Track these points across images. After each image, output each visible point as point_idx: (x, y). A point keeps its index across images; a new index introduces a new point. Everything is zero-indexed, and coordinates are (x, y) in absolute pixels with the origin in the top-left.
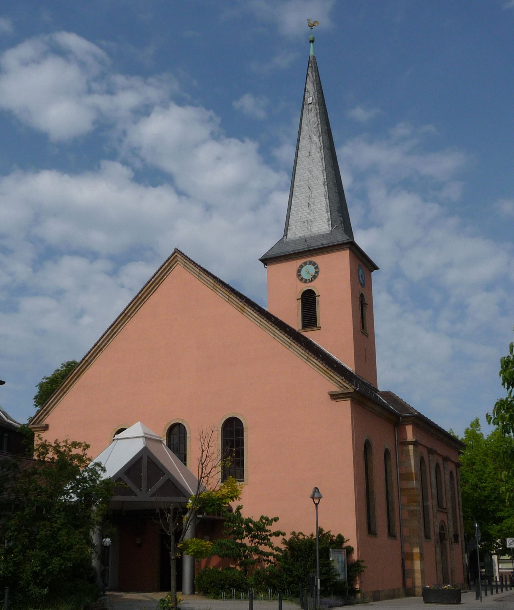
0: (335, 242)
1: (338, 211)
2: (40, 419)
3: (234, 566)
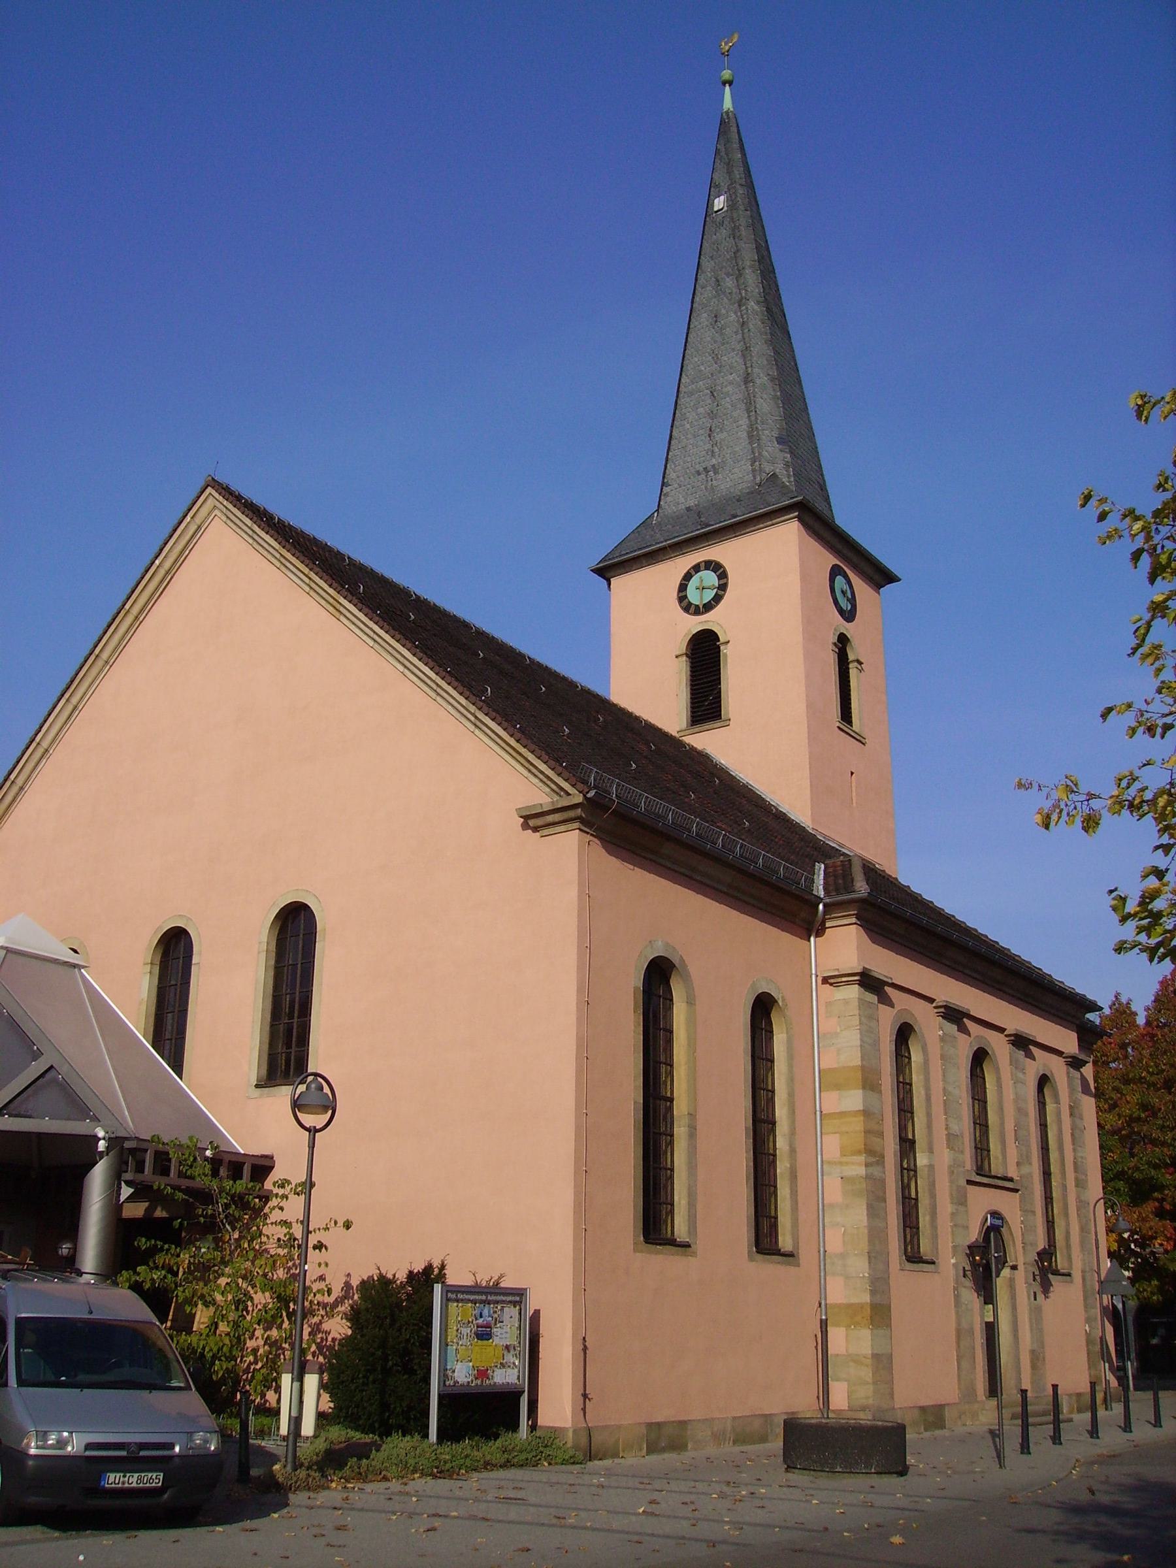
1: (780, 440)
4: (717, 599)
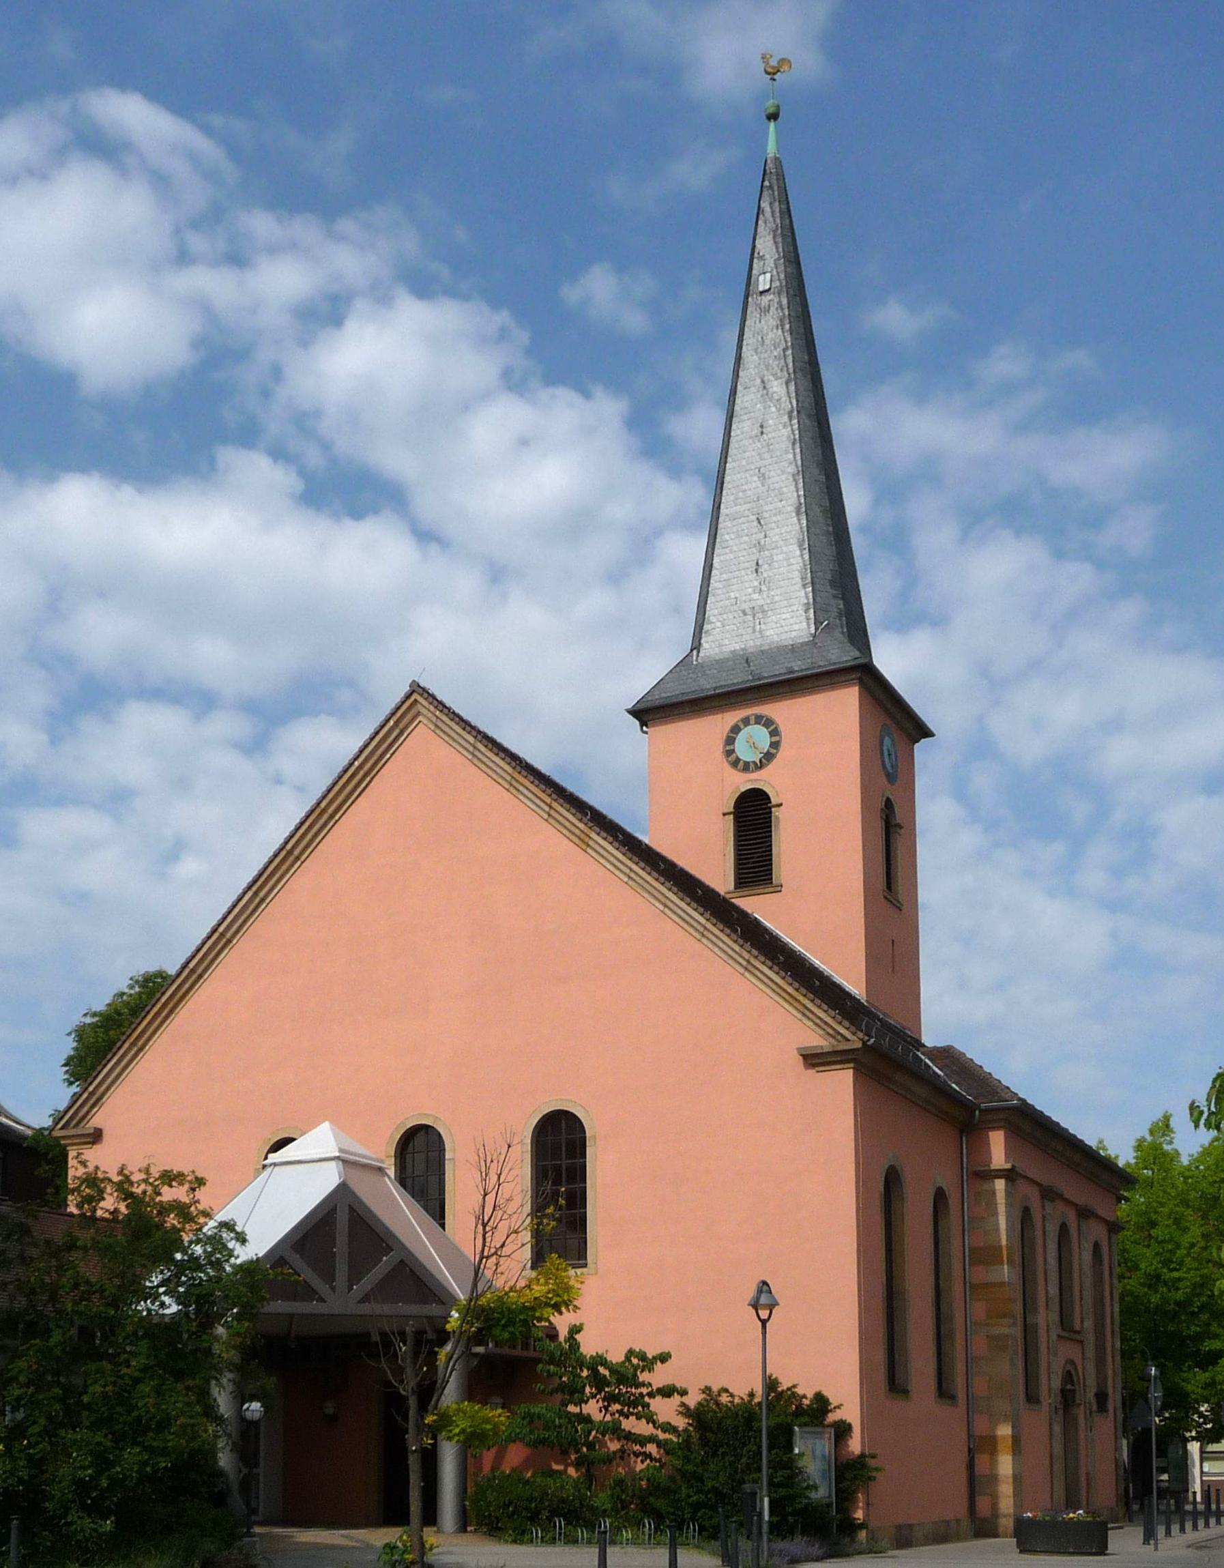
0: (822, 665)
2: (81, 1114)
3: (561, 1467)
4: (769, 757)
